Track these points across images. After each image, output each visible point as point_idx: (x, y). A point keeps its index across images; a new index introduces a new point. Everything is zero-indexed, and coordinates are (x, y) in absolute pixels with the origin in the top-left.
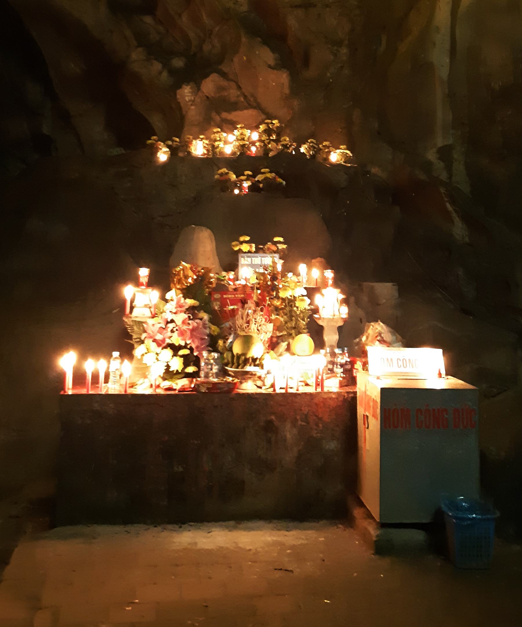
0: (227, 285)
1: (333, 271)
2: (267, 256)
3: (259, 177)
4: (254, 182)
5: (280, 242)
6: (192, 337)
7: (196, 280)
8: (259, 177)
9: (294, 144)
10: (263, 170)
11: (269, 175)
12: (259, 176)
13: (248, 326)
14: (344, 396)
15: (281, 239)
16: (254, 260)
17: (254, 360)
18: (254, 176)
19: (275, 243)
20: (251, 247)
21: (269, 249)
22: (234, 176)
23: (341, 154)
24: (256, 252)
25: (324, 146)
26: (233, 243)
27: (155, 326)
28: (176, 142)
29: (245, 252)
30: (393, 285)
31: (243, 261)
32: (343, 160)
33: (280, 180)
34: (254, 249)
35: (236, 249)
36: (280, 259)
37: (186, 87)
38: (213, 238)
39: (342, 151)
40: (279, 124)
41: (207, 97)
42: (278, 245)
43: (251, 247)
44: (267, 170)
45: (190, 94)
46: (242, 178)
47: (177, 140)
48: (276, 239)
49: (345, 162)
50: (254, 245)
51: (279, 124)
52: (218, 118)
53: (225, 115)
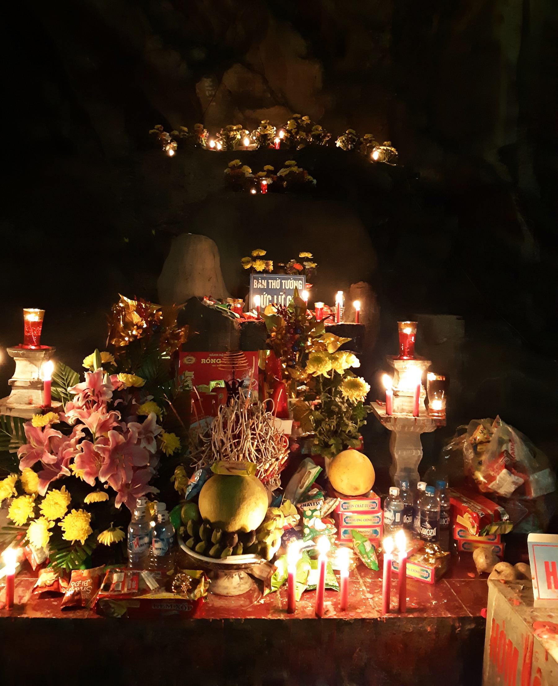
2: (290, 279)
3: (282, 172)
4: (275, 179)
5: (307, 259)
6: (113, 468)
7: (145, 330)
8: (282, 172)
9: (329, 134)
11: (295, 169)
12: (282, 170)
13: (239, 443)
14: (454, 628)
15: (309, 255)
16: (271, 283)
17: (244, 535)
18: (275, 172)
19: (302, 261)
20: (267, 265)
21: (292, 268)
23: (385, 151)
25: (365, 139)
26: (244, 259)
27: (45, 431)
28: (184, 131)
29: (260, 272)
30: (458, 319)
31: (256, 284)
32: (387, 159)
34: (271, 268)
35: (248, 267)
37: (205, 79)
38: (216, 249)
39: (385, 148)
40: (310, 121)
41: (230, 92)
42: (305, 263)
43: (267, 265)
44: (293, 162)
45: (210, 89)
46: (261, 173)
47: (186, 129)
48: (302, 255)
49: (388, 162)
50: (271, 263)
51: (310, 121)
52: (240, 116)
53: (248, 112)
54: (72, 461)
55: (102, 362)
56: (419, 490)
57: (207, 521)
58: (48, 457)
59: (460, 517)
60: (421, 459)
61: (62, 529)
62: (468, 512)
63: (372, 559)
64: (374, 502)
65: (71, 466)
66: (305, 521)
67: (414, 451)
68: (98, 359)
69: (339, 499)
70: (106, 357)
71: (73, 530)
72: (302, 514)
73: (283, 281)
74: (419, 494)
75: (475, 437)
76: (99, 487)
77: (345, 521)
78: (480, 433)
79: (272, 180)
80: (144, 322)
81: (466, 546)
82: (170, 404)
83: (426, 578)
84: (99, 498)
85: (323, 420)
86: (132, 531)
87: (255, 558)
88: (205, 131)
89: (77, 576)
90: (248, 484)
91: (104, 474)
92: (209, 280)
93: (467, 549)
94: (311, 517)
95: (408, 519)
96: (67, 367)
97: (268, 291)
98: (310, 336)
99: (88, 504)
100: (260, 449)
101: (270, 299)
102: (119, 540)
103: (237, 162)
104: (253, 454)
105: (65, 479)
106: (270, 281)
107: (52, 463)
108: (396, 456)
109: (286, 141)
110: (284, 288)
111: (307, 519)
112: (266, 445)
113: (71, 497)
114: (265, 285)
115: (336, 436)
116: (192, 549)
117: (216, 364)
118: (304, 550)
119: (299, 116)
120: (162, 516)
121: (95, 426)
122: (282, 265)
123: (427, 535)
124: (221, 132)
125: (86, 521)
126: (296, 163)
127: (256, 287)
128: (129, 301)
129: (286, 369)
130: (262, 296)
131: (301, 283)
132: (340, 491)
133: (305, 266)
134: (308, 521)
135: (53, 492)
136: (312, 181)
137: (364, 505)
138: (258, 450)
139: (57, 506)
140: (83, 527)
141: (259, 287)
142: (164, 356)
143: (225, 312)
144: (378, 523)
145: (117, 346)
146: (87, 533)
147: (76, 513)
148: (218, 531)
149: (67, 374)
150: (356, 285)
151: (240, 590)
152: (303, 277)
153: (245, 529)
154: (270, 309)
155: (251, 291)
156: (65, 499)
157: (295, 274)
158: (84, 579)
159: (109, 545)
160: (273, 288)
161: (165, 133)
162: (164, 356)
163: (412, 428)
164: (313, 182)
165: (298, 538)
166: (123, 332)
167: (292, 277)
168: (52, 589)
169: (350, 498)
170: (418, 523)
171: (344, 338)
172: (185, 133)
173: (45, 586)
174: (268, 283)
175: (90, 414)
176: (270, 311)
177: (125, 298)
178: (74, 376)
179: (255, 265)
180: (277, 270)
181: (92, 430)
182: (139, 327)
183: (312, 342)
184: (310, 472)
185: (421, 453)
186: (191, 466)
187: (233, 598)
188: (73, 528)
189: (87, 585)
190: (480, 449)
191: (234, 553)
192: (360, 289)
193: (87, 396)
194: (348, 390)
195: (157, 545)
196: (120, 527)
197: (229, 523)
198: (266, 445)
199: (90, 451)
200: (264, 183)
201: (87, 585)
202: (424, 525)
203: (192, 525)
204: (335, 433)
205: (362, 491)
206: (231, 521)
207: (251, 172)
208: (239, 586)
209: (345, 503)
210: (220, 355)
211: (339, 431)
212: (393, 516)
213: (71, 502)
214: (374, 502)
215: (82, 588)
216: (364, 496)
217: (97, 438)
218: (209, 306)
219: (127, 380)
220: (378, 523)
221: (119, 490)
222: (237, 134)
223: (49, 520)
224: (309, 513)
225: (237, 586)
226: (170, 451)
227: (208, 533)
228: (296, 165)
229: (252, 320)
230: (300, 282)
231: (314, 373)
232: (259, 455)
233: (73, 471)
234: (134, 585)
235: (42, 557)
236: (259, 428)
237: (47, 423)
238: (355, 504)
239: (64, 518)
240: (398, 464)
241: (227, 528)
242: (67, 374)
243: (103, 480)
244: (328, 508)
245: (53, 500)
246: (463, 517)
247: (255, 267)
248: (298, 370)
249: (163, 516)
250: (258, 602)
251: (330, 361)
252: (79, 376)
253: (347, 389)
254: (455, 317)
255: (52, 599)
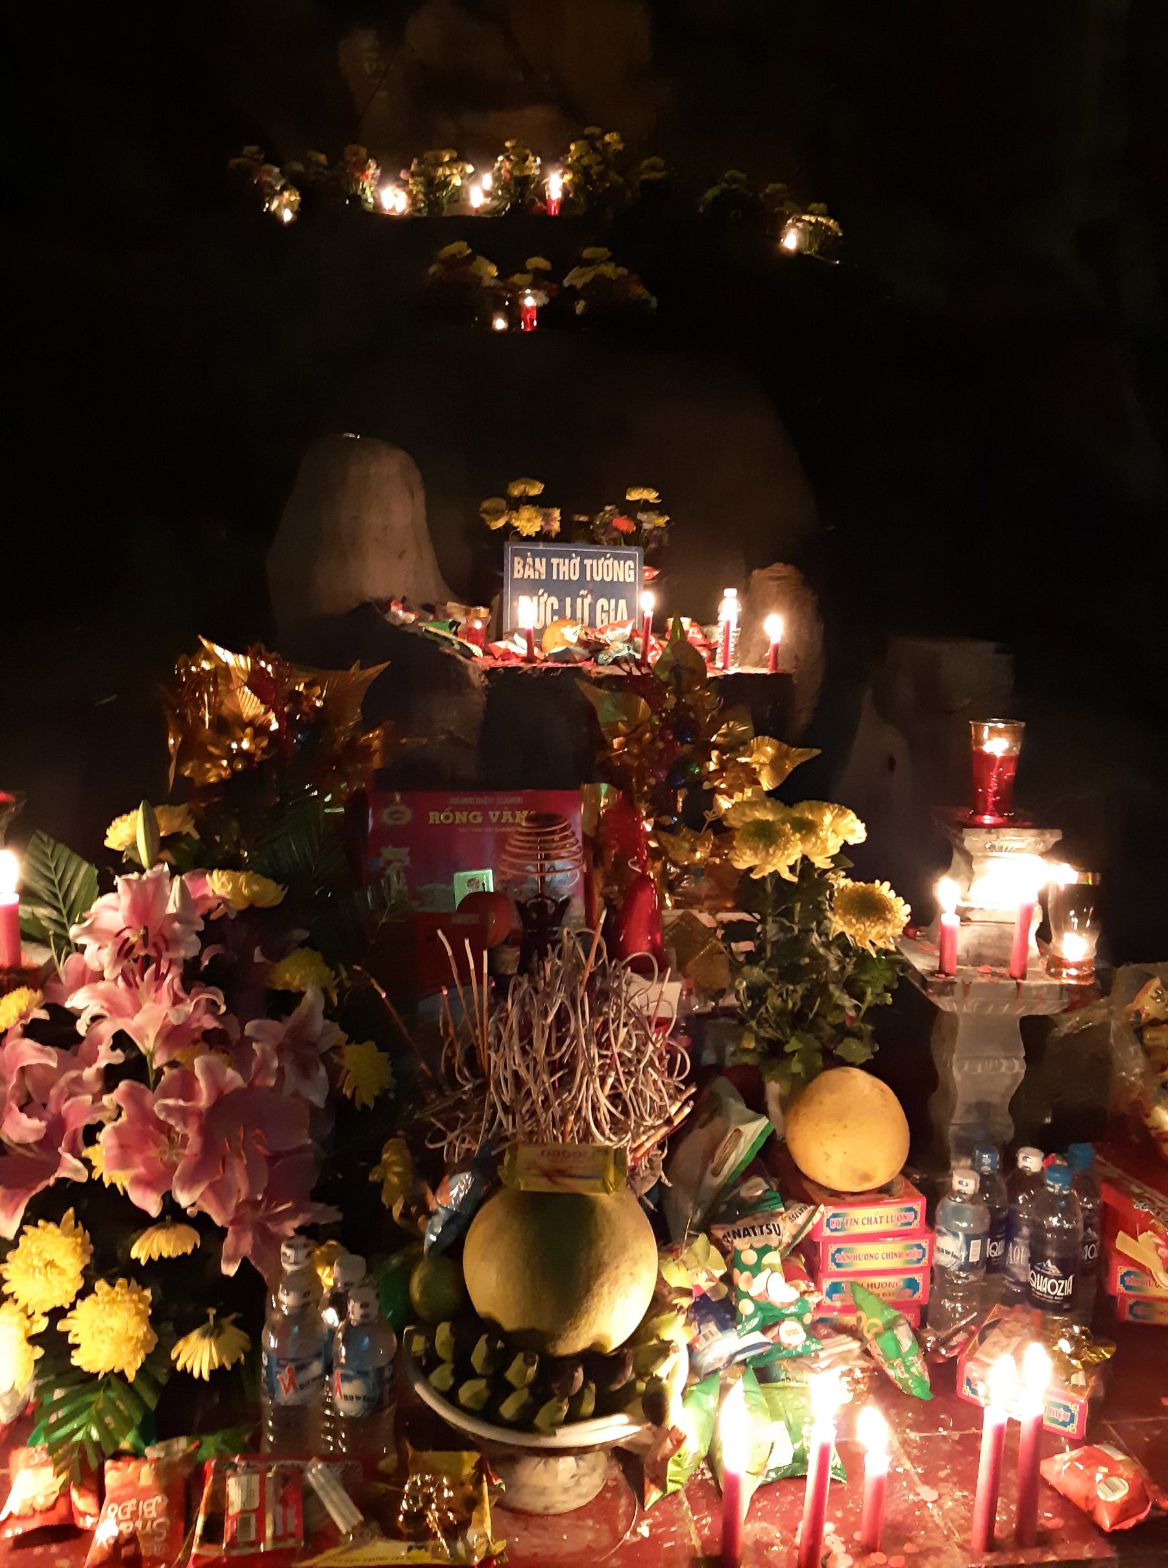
0: (462, 658)
1: (1023, 724)
2: (604, 555)
3: (575, 278)
5: (645, 506)
10: (587, 253)
11: (609, 270)
12: (575, 271)
15: (651, 496)
16: (558, 565)
19: (632, 510)
21: (607, 526)
22: (493, 271)
23: (811, 228)
24: (565, 537)
25: (768, 196)
26: (486, 505)
28: (318, 164)
29: (528, 539)
30: (998, 651)
31: (520, 568)
32: (816, 247)
33: (641, 291)
34: (556, 526)
36: (646, 563)
38: (416, 476)
39: (813, 219)
42: (642, 516)
43: (547, 518)
44: (603, 252)
46: (517, 278)
47: (323, 158)
48: (634, 495)
49: (817, 252)
50: (557, 513)
54: (90, 1135)
55: (162, 834)
56: (1022, 1172)
57: (490, 1326)
58: (18, 1124)
59: (1129, 1238)
60: (1020, 1082)
61: (71, 1340)
62: (1154, 1229)
63: (913, 1370)
64: (911, 1209)
65: (88, 1152)
66: (741, 1279)
67: (1004, 1062)
68: (151, 825)
69: (822, 1207)
70: (170, 822)
71: (103, 1341)
72: (732, 1259)
73: (588, 562)
74: (1019, 1180)
75: (1138, 1007)
76: (172, 1214)
77: (834, 1260)
78: (1152, 998)
79: (548, 295)
80: (272, 716)
81: (1138, 1310)
82: (384, 995)
83: (1064, 1424)
84: (175, 1246)
85: (768, 985)
86: (273, 1343)
87: (630, 1423)
88: (372, 164)
89: (124, 1486)
90: (608, 1221)
91: (190, 1181)
92: (400, 557)
93: (1144, 1317)
94: (756, 1269)
95: (994, 1248)
96: (60, 846)
97: (551, 586)
98: (715, 746)
99: (143, 1262)
100: (620, 1094)
101: (556, 607)
102: (234, 1361)
103: (460, 248)
104: (603, 1109)
105: (70, 1186)
106: (554, 561)
107: (31, 1139)
108: (957, 1075)
109: (575, 195)
110: (588, 578)
111: (747, 1274)
112: (636, 1082)
113: (92, 1242)
114: (543, 570)
115: (802, 1029)
116: (450, 1397)
117: (468, 824)
118: (740, 1358)
119: (597, 131)
120: (362, 1306)
121: (152, 1033)
122: (582, 519)
123: (1048, 1293)
124: (413, 168)
125: (138, 1313)
126: (609, 254)
127: (520, 576)
128: (226, 656)
129: (654, 835)
130: (535, 598)
131: (632, 567)
132: (822, 1180)
133: (641, 522)
134: (748, 1282)
135: (39, 1232)
136: (647, 302)
137: (882, 1216)
138: (615, 1097)
139: (52, 1274)
140: (131, 1333)
141: (526, 577)
142: (328, 805)
143: (446, 643)
144: (919, 1261)
145: (197, 784)
146: (142, 1347)
147: (108, 1294)
148: (530, 1360)
149: (62, 867)
150: (766, 573)
151: (580, 1496)
152: (636, 552)
153: (603, 1346)
154: (557, 634)
155: (508, 589)
156: (74, 1249)
157: (615, 543)
158: (143, 1494)
159: (206, 1376)
160: (561, 578)
161: (268, 166)
162: (328, 805)
163: (1007, 1006)
164: (650, 302)
165: (723, 1326)
166: (215, 745)
167: (609, 552)
168: (53, 1519)
169: (849, 1199)
170: (1019, 1255)
171: (800, 750)
172: (321, 170)
173: (31, 1513)
174: (549, 566)
175: (138, 1007)
176: (558, 639)
177: (219, 650)
178: (82, 873)
179: (517, 519)
180: (570, 535)
181: (144, 1045)
182: (260, 730)
183: (721, 762)
184: (738, 1130)
185: (1021, 1067)
186: (431, 1146)
187: (565, 1522)
188: (101, 1337)
189: (154, 1514)
190: (1150, 1039)
191: (574, 1418)
192: (775, 583)
193: (127, 946)
194: (854, 921)
195: (347, 1389)
196: (233, 1317)
197: (560, 1336)
198: (636, 1082)
199: (144, 1115)
200: (530, 302)
201: (154, 1514)
202: (1041, 1267)
203: (453, 1340)
204: (798, 1020)
205: (879, 1180)
206: (565, 1329)
207: (496, 274)
208: (578, 1484)
209: (835, 1216)
210: (480, 801)
211: (811, 1016)
212: (964, 1247)
213: (93, 1256)
214: (911, 1209)
215: (139, 1524)
216: (884, 1192)
217: (160, 1072)
218: (404, 624)
219: (236, 890)
220: (919, 1261)
221: (232, 1223)
222: (452, 174)
223: (30, 1312)
224: (750, 1257)
225: (572, 1483)
226: (367, 1097)
227: (499, 1361)
228: (610, 260)
229: (513, 663)
230: (630, 563)
231: (751, 870)
232: (616, 1107)
233: (94, 1167)
234: (293, 1523)
235: (13, 1404)
236: (621, 1040)
237: (13, 1021)
238: (866, 1218)
239: (73, 1306)
240: (959, 1093)
241: (553, 1347)
242: (62, 867)
243: (184, 1199)
244: (794, 1232)
245: (39, 1254)
246: (1136, 1239)
247: (516, 524)
248: (684, 839)
249: (364, 1306)
250: (634, 1533)
251: (798, 836)
252: (96, 872)
253: (849, 917)
254: (992, 646)
255: (54, 1549)
